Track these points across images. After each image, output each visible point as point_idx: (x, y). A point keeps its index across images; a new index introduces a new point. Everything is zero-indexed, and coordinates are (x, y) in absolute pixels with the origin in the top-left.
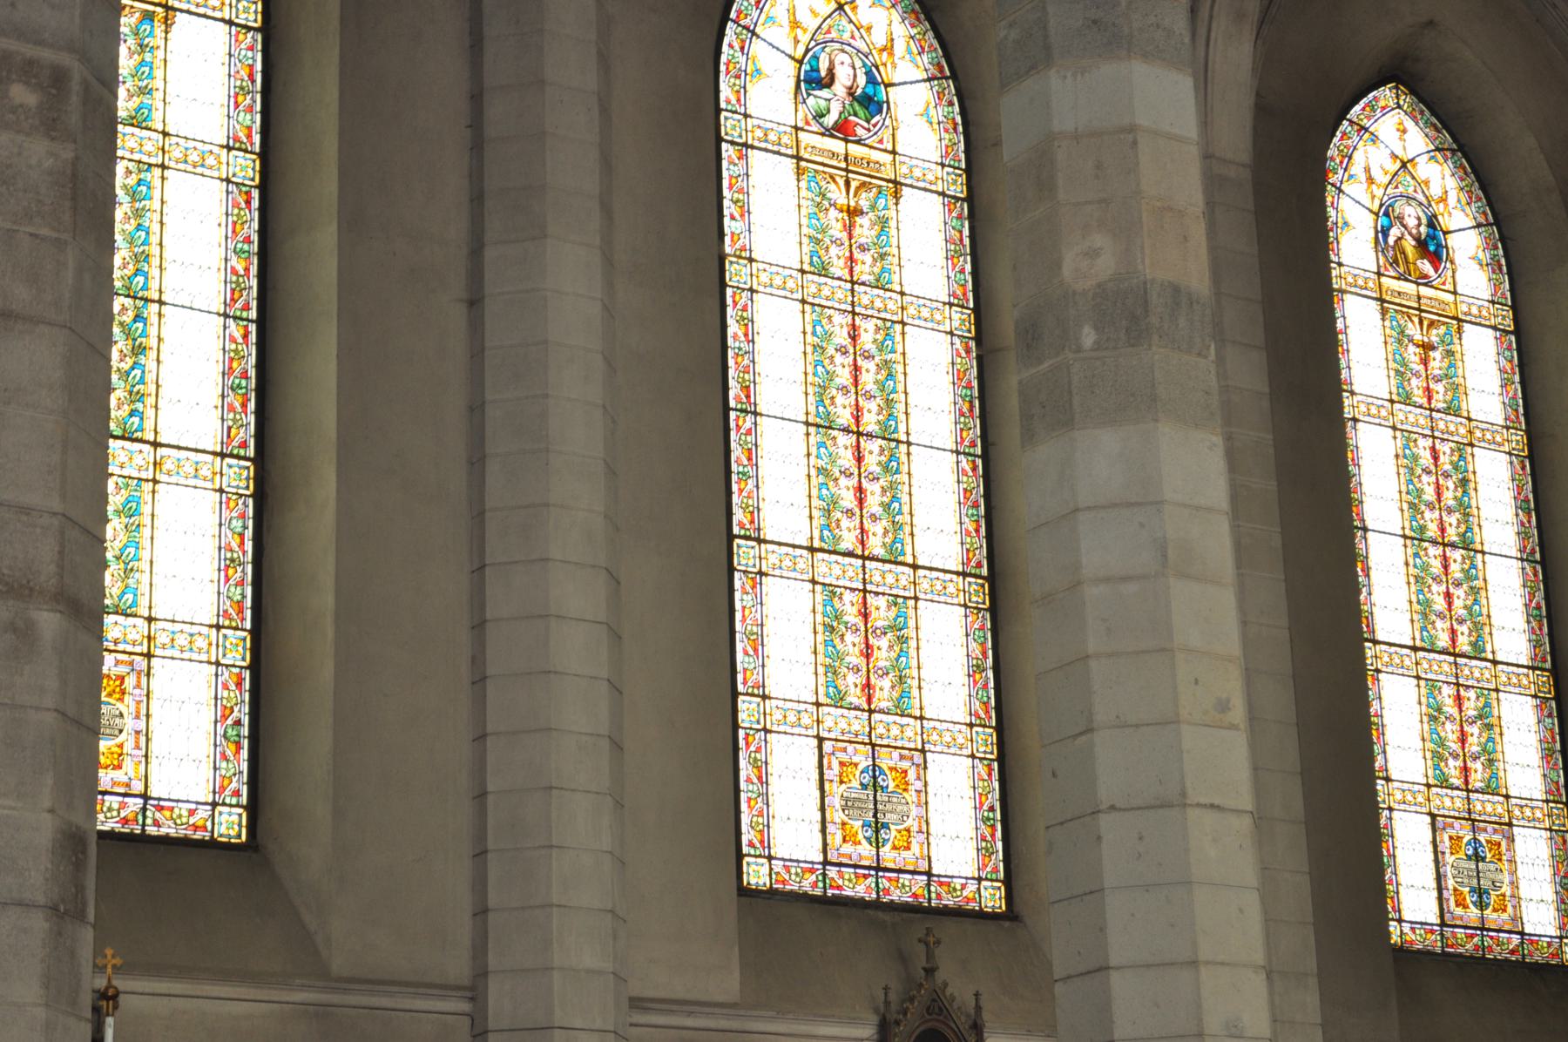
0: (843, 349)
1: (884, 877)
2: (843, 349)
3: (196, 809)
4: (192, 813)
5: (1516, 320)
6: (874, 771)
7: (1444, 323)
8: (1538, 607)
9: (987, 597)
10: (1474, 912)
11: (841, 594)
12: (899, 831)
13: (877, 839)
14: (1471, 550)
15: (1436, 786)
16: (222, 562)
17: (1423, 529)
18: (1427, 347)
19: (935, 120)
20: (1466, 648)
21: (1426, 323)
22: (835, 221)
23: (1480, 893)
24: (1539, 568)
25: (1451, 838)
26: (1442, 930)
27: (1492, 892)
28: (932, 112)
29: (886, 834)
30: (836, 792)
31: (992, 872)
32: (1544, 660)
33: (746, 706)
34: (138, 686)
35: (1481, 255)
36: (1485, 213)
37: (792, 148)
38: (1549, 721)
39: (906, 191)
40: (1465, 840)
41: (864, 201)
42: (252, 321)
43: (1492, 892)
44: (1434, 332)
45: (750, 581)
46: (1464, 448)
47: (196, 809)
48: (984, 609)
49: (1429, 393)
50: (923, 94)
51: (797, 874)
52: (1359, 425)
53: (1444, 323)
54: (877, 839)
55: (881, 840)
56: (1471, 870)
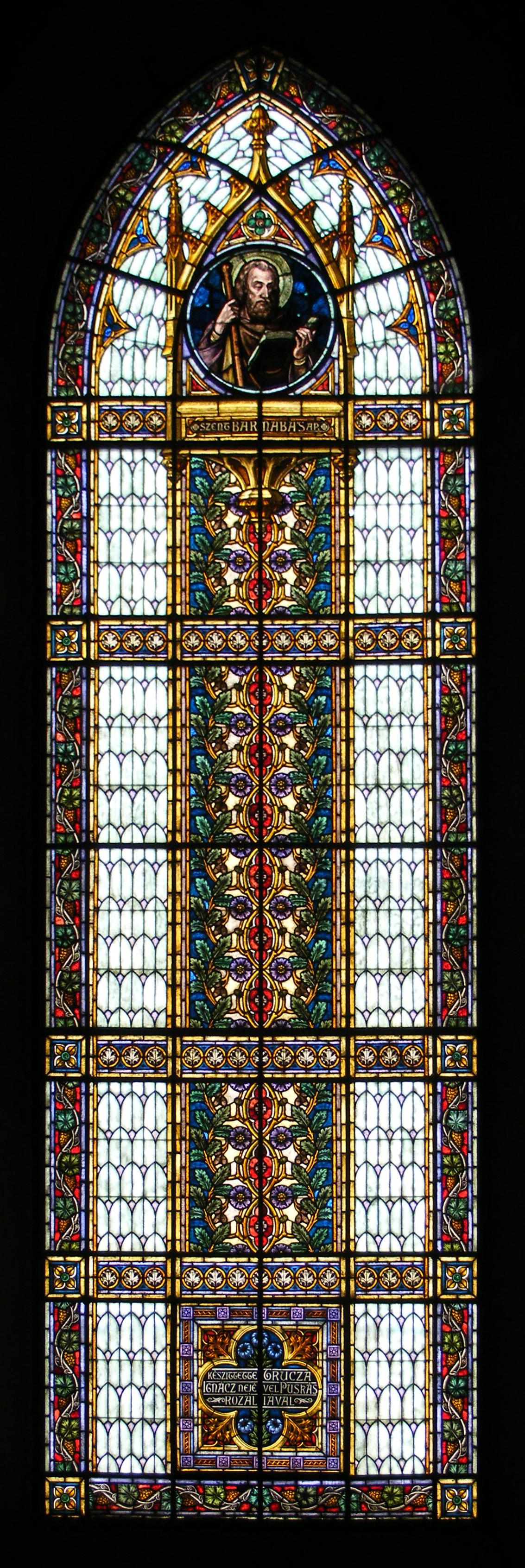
0: (241, 724)
1: (272, 1487)
2: (241, 724)
3: (413, 1485)
4: (406, 1490)
6: (260, 1338)
7: (311, 458)
9: (475, 1060)
11: (220, 1091)
12: (297, 1420)
13: (260, 1433)
14: (324, 846)
15: (191, 1254)
16: (439, 1171)
17: (218, 826)
19: (422, 328)
25: (205, 1333)
26: (173, 1484)
27: (286, 1415)
28: (419, 317)
29: (276, 1425)
31: (458, 1463)
34: (333, 1342)
37: (164, 431)
38: (457, 1119)
40: (238, 1335)
42: (472, 845)
43: (286, 1415)
45: (69, 1092)
47: (413, 1485)
48: (467, 1079)
51: (216, 1495)
53: (311, 458)
54: (260, 1433)
55: (265, 1435)
56: (247, 1382)
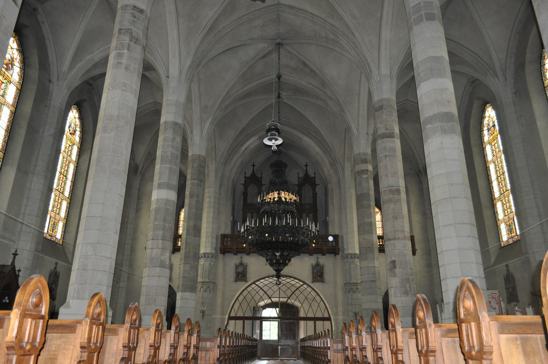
5: (21, 88)
8: (6, 140)
10: (51, 233)
18: (70, 146)
20: (61, 192)
21: (4, 78)
22: (68, 146)
23: (53, 230)
24: (8, 134)
30: (51, 223)
32: (3, 151)
33: (232, 322)
35: (19, 73)
36: (22, 67)
39: (12, 84)
41: (5, 81)
44: (5, 80)
46: (69, 162)
49: (68, 152)
50: (18, 70)
52: (5, 106)
